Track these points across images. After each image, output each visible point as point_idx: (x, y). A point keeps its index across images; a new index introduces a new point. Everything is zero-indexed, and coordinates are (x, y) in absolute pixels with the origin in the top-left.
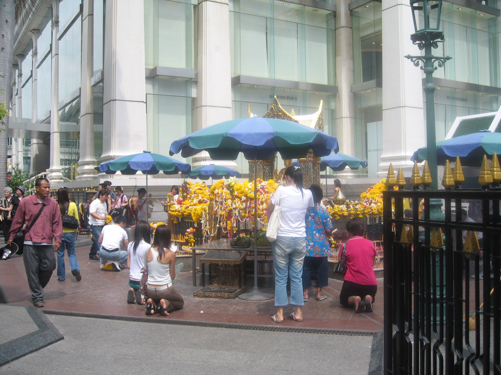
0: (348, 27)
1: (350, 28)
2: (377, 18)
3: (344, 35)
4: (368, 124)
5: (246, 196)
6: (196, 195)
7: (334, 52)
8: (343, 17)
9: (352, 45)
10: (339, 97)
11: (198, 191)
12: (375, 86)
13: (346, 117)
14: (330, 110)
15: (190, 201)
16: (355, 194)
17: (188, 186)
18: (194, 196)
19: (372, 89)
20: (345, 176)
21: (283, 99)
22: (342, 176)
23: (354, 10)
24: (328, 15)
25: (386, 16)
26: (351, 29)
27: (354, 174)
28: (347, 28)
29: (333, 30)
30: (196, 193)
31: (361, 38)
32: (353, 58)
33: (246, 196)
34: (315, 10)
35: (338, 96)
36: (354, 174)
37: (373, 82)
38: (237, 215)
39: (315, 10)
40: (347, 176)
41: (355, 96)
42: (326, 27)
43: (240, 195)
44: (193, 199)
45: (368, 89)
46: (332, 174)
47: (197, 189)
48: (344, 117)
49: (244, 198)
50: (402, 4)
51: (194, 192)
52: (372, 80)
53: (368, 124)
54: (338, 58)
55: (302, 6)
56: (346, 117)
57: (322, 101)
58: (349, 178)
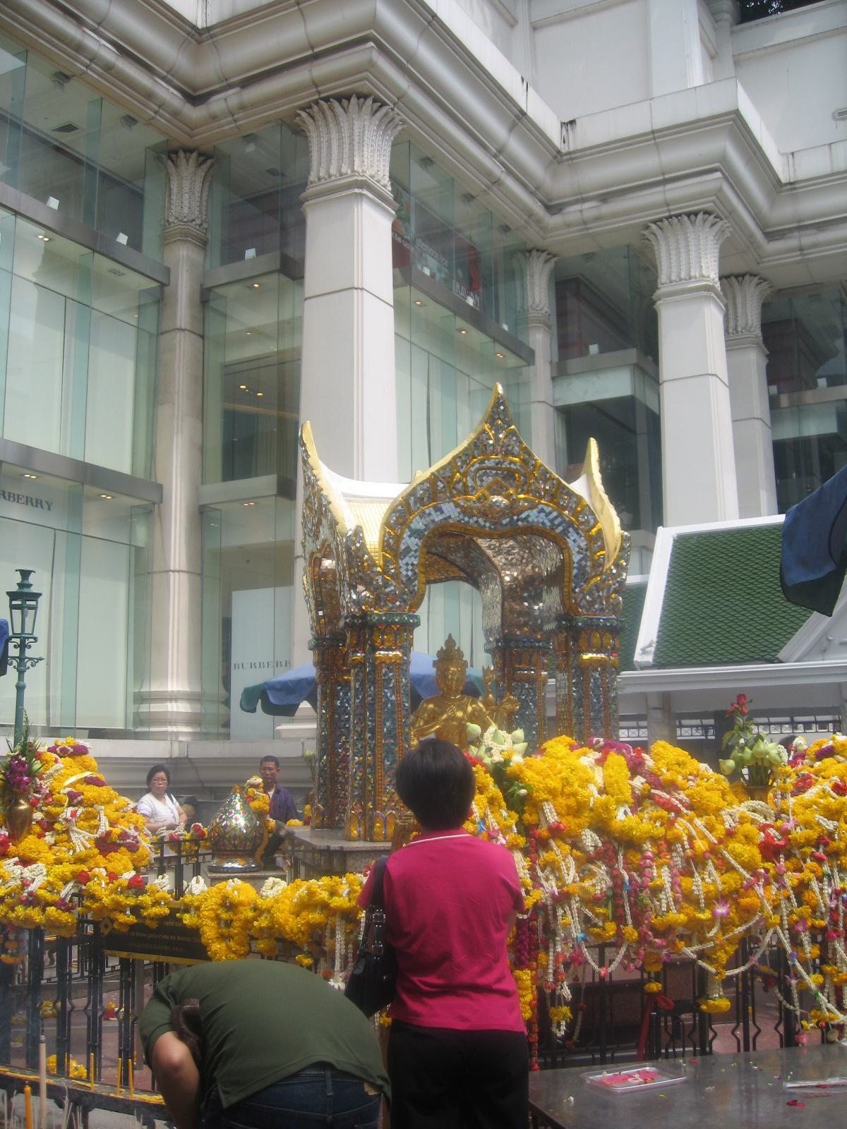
0: (194, 333)
1: (199, 335)
2: (286, 315)
3: (182, 349)
4: (234, 593)
5: (601, 827)
6: (80, 810)
7: (152, 394)
8: (184, 304)
9: (201, 380)
10: (160, 515)
11: (90, 792)
12: (275, 492)
13: (178, 571)
14: (133, 549)
15: (49, 838)
16: (206, 785)
17: (37, 765)
18: (74, 814)
19: (256, 500)
20: (172, 733)
21: (15, 503)
22: (165, 733)
23: (220, 291)
24: (144, 292)
25: (316, 318)
26: (200, 339)
27: (198, 730)
28: (193, 336)
29: (151, 335)
30: (80, 803)
31: (227, 366)
32: (201, 414)
33: (601, 827)
34: (115, 272)
35: (156, 512)
36: (198, 730)
37: (265, 483)
38: (577, 933)
39: (115, 272)
40: (177, 734)
41: (202, 516)
42: (134, 322)
43: (569, 823)
44: (67, 832)
45: (248, 500)
46: (130, 728)
47: (79, 781)
48: (172, 569)
49: (590, 839)
50: (362, 289)
51: (72, 796)
52: (267, 474)
53: (234, 593)
54: (163, 411)
55: (90, 251)
56: (178, 571)
57: (593, 444)
58: (181, 738)
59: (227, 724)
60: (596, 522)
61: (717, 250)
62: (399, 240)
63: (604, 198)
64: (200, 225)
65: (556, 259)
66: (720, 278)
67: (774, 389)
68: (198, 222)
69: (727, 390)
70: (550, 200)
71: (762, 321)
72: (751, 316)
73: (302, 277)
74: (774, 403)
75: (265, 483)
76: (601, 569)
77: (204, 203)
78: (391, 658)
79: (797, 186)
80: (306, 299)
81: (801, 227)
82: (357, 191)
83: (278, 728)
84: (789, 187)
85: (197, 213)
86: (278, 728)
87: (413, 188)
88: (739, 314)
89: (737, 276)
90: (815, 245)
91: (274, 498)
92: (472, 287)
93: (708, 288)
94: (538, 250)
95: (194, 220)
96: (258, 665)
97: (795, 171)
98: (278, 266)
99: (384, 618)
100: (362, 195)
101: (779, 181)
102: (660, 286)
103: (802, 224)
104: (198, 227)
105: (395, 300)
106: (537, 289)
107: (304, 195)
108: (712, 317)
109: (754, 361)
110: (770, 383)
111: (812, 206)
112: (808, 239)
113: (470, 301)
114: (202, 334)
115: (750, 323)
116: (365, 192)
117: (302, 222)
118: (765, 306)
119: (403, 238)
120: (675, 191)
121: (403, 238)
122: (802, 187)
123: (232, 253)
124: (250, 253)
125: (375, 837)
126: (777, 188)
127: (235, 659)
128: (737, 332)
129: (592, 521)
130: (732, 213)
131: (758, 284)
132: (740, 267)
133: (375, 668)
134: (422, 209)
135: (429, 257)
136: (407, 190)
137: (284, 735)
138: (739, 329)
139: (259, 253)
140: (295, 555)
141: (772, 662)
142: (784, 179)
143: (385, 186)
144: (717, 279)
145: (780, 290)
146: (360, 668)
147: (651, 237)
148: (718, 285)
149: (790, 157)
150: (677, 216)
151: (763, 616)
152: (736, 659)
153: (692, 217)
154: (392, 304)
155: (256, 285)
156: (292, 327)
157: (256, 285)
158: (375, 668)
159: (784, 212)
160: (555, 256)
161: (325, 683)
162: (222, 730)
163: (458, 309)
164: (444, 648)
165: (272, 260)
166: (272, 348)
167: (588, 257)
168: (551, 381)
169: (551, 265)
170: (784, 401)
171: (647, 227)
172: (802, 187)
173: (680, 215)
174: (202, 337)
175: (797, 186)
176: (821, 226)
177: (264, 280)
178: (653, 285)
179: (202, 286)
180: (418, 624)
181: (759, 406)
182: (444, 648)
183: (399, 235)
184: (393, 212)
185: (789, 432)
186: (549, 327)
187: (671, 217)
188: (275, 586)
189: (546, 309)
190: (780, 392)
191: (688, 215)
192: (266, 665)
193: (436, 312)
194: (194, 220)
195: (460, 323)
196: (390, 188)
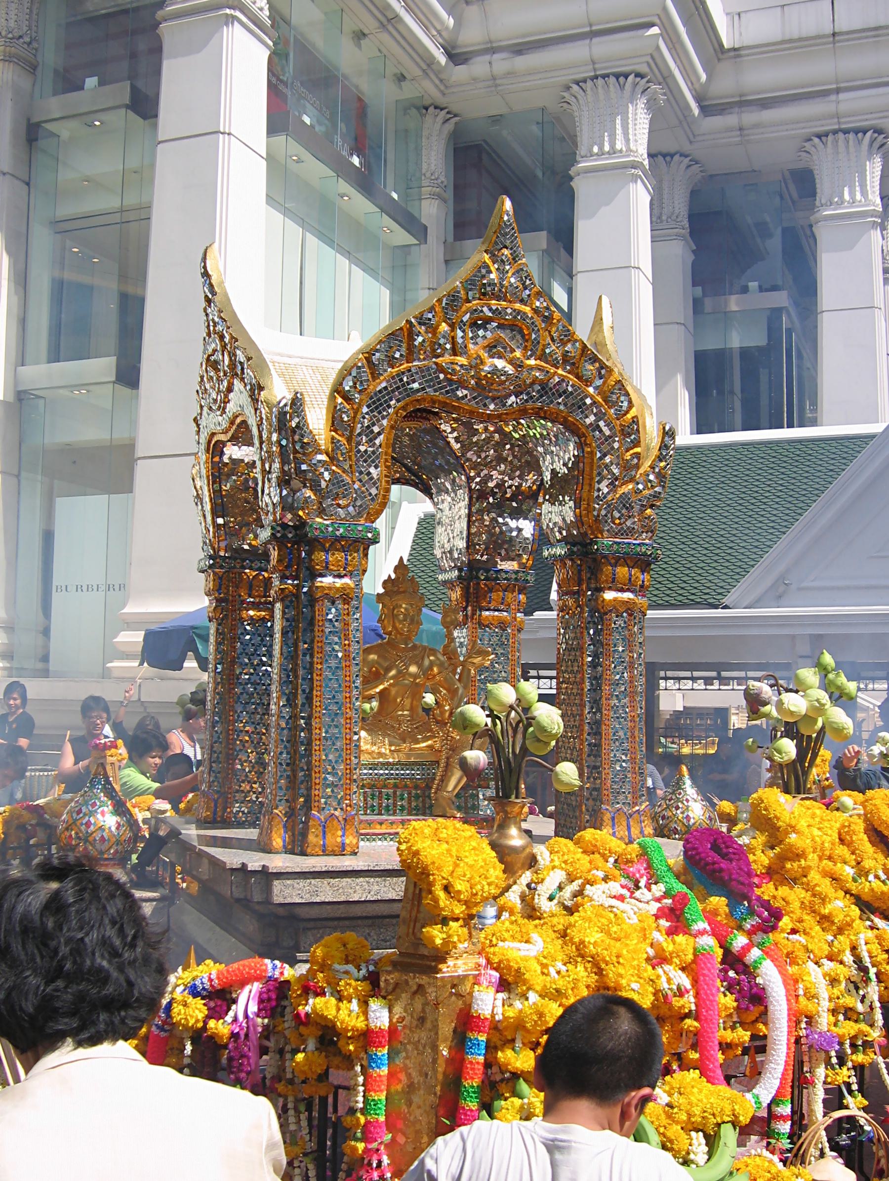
0: (17, 178)
2: (133, 162)
12: (113, 379)
23: (47, 126)
25: (170, 165)
28: (17, 182)
59: (45, 659)
60: (631, 405)
61: (647, 121)
62: (274, 80)
63: (519, 49)
64: (29, 44)
65: (457, 119)
66: (651, 156)
67: (699, 290)
68: (27, 39)
69: (651, 287)
70: (454, 47)
71: (690, 210)
72: (680, 205)
73: (156, 116)
74: (697, 306)
75: (102, 367)
76: (633, 473)
77: (35, 17)
78: (338, 589)
79: (742, 52)
80: (160, 143)
81: (743, 103)
82: (228, 11)
83: (109, 665)
84: (732, 54)
85: (25, 29)
86: (109, 665)
87: (294, 21)
88: (665, 196)
89: (664, 156)
90: (756, 126)
91: (111, 385)
92: (358, 149)
93: (635, 165)
94: (436, 108)
95: (21, 37)
96: (85, 588)
97: (741, 34)
98: (127, 100)
99: (330, 529)
100: (234, 18)
101: (721, 45)
102: (578, 158)
103: (744, 98)
104: (25, 46)
105: (267, 154)
106: (433, 153)
107: (160, 14)
108: (640, 197)
109: (679, 252)
110: (694, 284)
111: (760, 78)
112: (750, 117)
113: (356, 160)
114: (27, 180)
115: (677, 211)
116: (238, 14)
117: (157, 50)
118: (694, 194)
119: (278, 79)
120: (603, 48)
121: (278, 79)
122: (748, 55)
123: (69, 82)
124: (91, 82)
125: (309, 850)
126: (717, 53)
127: (57, 579)
128: (662, 222)
129: (625, 404)
130: (667, 79)
131: (689, 166)
132: (669, 146)
133: (312, 600)
134: (304, 48)
135: (308, 105)
136: (288, 23)
137: (115, 674)
138: (664, 218)
139: (101, 83)
140: (136, 456)
141: (716, 607)
142: (726, 45)
143: (261, 9)
144: (646, 156)
145: (711, 176)
146: (291, 601)
147: (572, 100)
148: (646, 163)
149: (736, 17)
150: (604, 76)
151: (705, 552)
152: (673, 602)
153: (622, 79)
154: (265, 156)
155: (97, 123)
156: (142, 176)
157: (97, 123)
158: (312, 600)
159: (726, 85)
160: (455, 116)
161: (222, 619)
162: (40, 665)
163: (342, 169)
164: (393, 576)
165: (122, 92)
166: (112, 202)
167: (496, 119)
168: (443, 266)
169: (450, 126)
170: (709, 303)
171: (568, 88)
172: (748, 55)
173: (607, 75)
174: (28, 184)
175: (742, 52)
176: (765, 104)
177: (107, 117)
178: (571, 159)
179: (29, 120)
180: (375, 541)
181: (681, 310)
182: (393, 576)
183: (274, 75)
184: (271, 43)
185: (711, 343)
186: (445, 201)
187: (596, 77)
188: (109, 492)
189: (442, 179)
190: (705, 295)
191: (617, 76)
192: (95, 588)
193: (316, 170)
194: (21, 37)
195: (344, 186)
196: (268, 13)
